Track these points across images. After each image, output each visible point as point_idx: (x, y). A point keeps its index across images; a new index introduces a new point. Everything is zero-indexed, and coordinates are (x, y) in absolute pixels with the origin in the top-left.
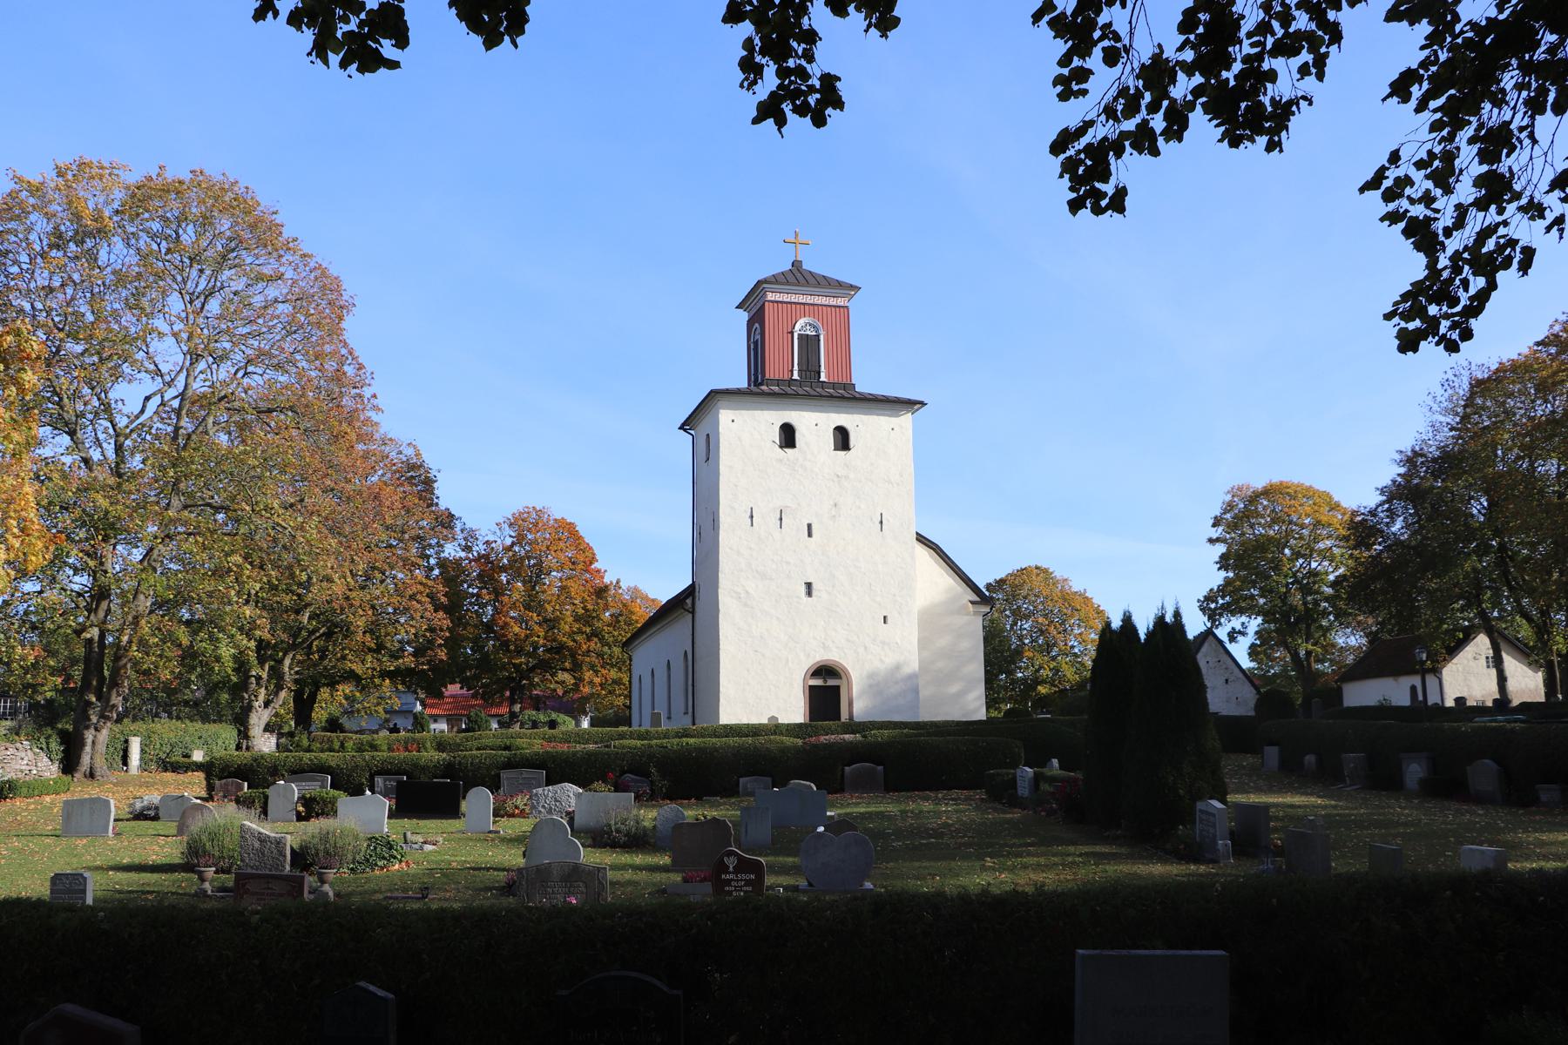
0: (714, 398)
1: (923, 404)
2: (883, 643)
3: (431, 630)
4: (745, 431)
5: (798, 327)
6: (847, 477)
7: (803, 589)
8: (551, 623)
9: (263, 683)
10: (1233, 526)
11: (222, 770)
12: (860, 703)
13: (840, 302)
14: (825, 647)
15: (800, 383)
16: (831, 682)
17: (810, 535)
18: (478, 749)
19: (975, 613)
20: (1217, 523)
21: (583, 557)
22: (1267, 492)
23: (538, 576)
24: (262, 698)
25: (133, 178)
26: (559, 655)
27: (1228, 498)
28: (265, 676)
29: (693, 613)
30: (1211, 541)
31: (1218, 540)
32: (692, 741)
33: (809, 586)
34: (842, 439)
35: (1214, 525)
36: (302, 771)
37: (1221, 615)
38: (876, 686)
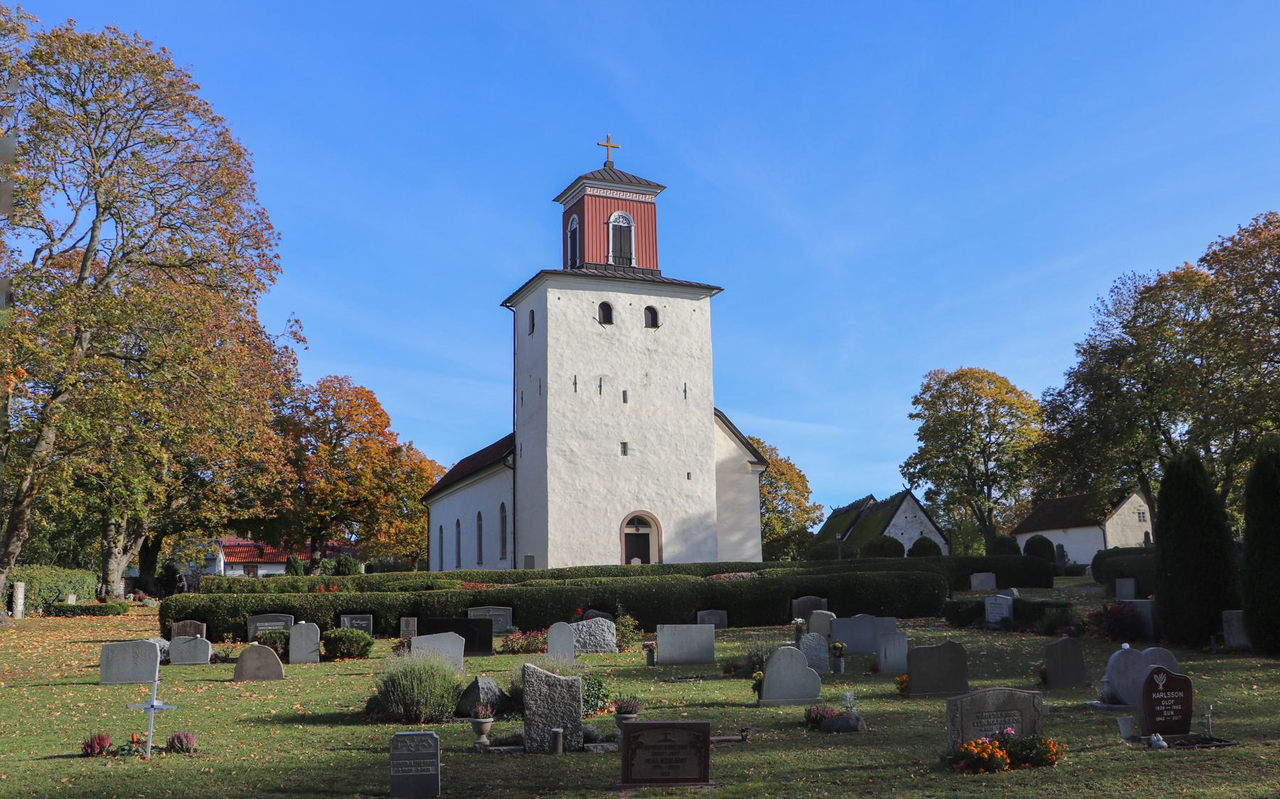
1: (720, 289)
2: (687, 496)
3: (283, 482)
4: (568, 308)
5: (612, 219)
7: (619, 449)
8: (354, 479)
9: (122, 531)
10: (931, 405)
11: (178, 612)
12: (669, 547)
13: (648, 198)
14: (638, 499)
15: (615, 268)
16: (642, 531)
17: (625, 401)
19: (753, 472)
20: (916, 401)
21: (379, 422)
22: (958, 377)
23: (339, 436)
24: (120, 545)
25: (49, 25)
26: (362, 509)
27: (925, 381)
28: (124, 524)
29: (514, 469)
30: (911, 416)
31: (918, 416)
32: (604, 579)
33: (624, 445)
34: (652, 318)
35: (914, 403)
36: (265, 612)
37: (919, 478)
38: (686, 530)
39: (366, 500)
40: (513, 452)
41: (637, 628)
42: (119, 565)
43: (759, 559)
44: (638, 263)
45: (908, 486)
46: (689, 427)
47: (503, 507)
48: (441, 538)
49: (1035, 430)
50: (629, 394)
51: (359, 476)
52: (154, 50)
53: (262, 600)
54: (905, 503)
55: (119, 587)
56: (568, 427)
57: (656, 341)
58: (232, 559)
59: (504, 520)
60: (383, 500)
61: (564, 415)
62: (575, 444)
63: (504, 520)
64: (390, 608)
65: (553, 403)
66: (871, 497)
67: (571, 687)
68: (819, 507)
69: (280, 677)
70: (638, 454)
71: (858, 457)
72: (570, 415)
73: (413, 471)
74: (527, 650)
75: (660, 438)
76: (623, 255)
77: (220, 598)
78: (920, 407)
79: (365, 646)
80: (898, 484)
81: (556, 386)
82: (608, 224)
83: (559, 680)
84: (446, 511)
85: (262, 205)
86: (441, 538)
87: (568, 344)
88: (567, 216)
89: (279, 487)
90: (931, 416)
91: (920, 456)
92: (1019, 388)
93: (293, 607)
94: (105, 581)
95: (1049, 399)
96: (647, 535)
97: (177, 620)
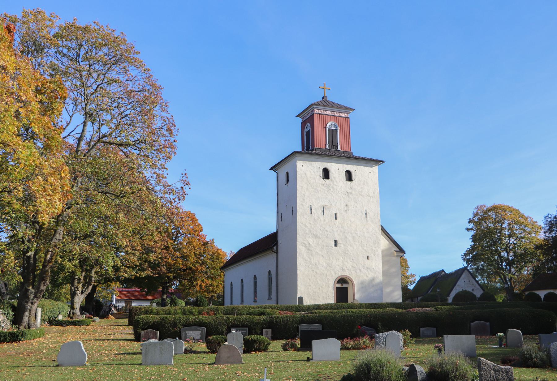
0: (294, 153)
1: (383, 162)
2: (367, 268)
4: (307, 170)
5: (328, 125)
6: (351, 193)
7: (333, 243)
8: (185, 257)
11: (144, 325)
12: (357, 296)
13: (346, 115)
14: (343, 270)
16: (345, 286)
17: (336, 218)
18: (247, 314)
19: (397, 256)
21: (197, 230)
22: (494, 208)
24: (80, 289)
25: (62, 22)
26: (187, 274)
29: (277, 253)
30: (468, 229)
31: (471, 229)
32: (353, 310)
33: (336, 241)
34: (349, 176)
35: (469, 222)
38: (364, 286)
39: (190, 268)
40: (277, 244)
41: (411, 336)
42: (79, 300)
43: (400, 301)
44: (341, 148)
45: (466, 265)
46: (368, 232)
47: (270, 273)
48: (232, 289)
49: (541, 236)
50: (338, 215)
51: (188, 256)
52: (116, 34)
53: (189, 319)
54: (464, 274)
55: (78, 311)
56: (308, 232)
57: (351, 188)
58: (119, 298)
59: (270, 279)
60: (200, 269)
61: (305, 226)
62: (311, 241)
63: (270, 279)
64: (257, 324)
65: (300, 219)
66: (443, 271)
67: (508, 372)
68: (413, 276)
69: (240, 362)
70: (342, 246)
71: (443, 250)
72: (308, 225)
73: (214, 254)
74: (355, 348)
75: (354, 238)
76: (333, 144)
77: (166, 318)
78: (472, 224)
79: (267, 345)
80: (461, 264)
81: (301, 211)
82: (326, 128)
83: (501, 368)
84: (235, 275)
85: (171, 114)
86: (232, 289)
87: (307, 189)
88: (303, 124)
89: (160, 260)
90: (478, 229)
91: (473, 249)
92: (526, 215)
93: (205, 323)
94: (72, 308)
95: (549, 220)
96: (347, 288)
97: (144, 329)
